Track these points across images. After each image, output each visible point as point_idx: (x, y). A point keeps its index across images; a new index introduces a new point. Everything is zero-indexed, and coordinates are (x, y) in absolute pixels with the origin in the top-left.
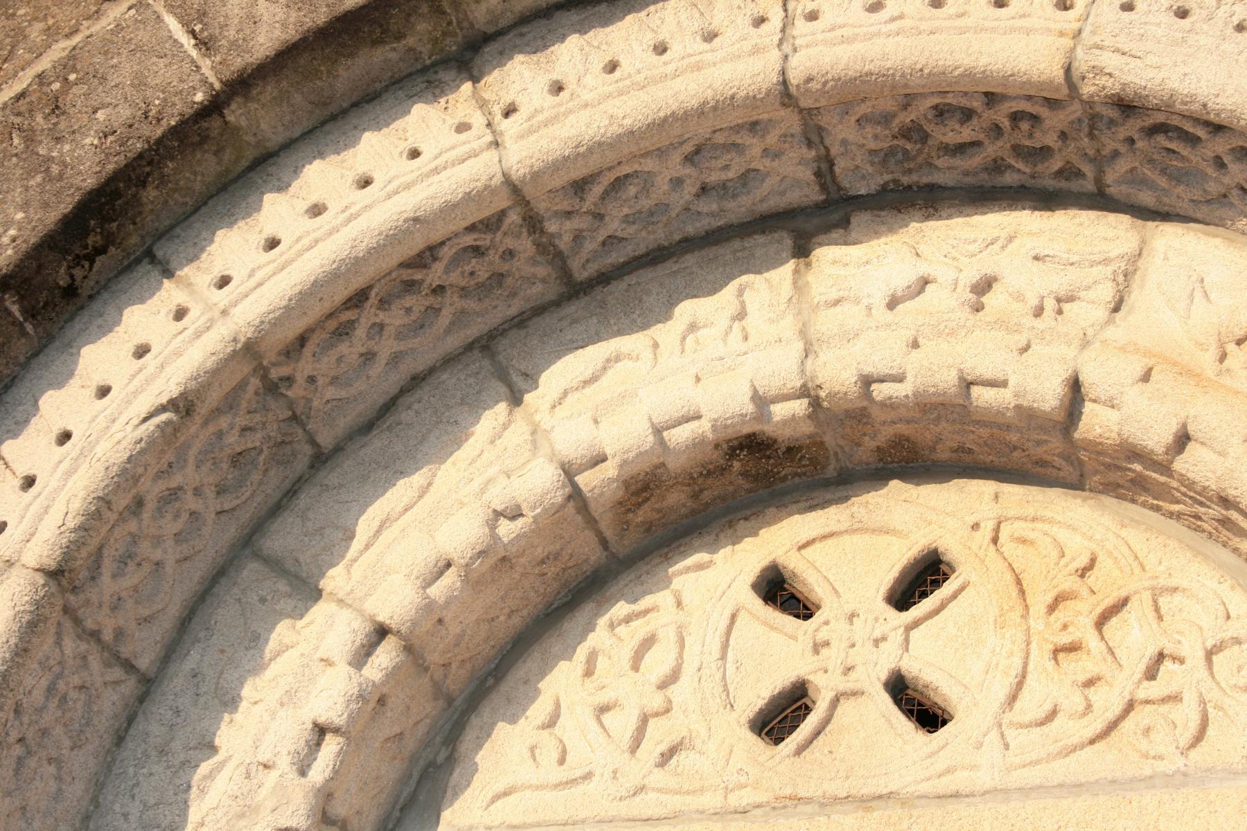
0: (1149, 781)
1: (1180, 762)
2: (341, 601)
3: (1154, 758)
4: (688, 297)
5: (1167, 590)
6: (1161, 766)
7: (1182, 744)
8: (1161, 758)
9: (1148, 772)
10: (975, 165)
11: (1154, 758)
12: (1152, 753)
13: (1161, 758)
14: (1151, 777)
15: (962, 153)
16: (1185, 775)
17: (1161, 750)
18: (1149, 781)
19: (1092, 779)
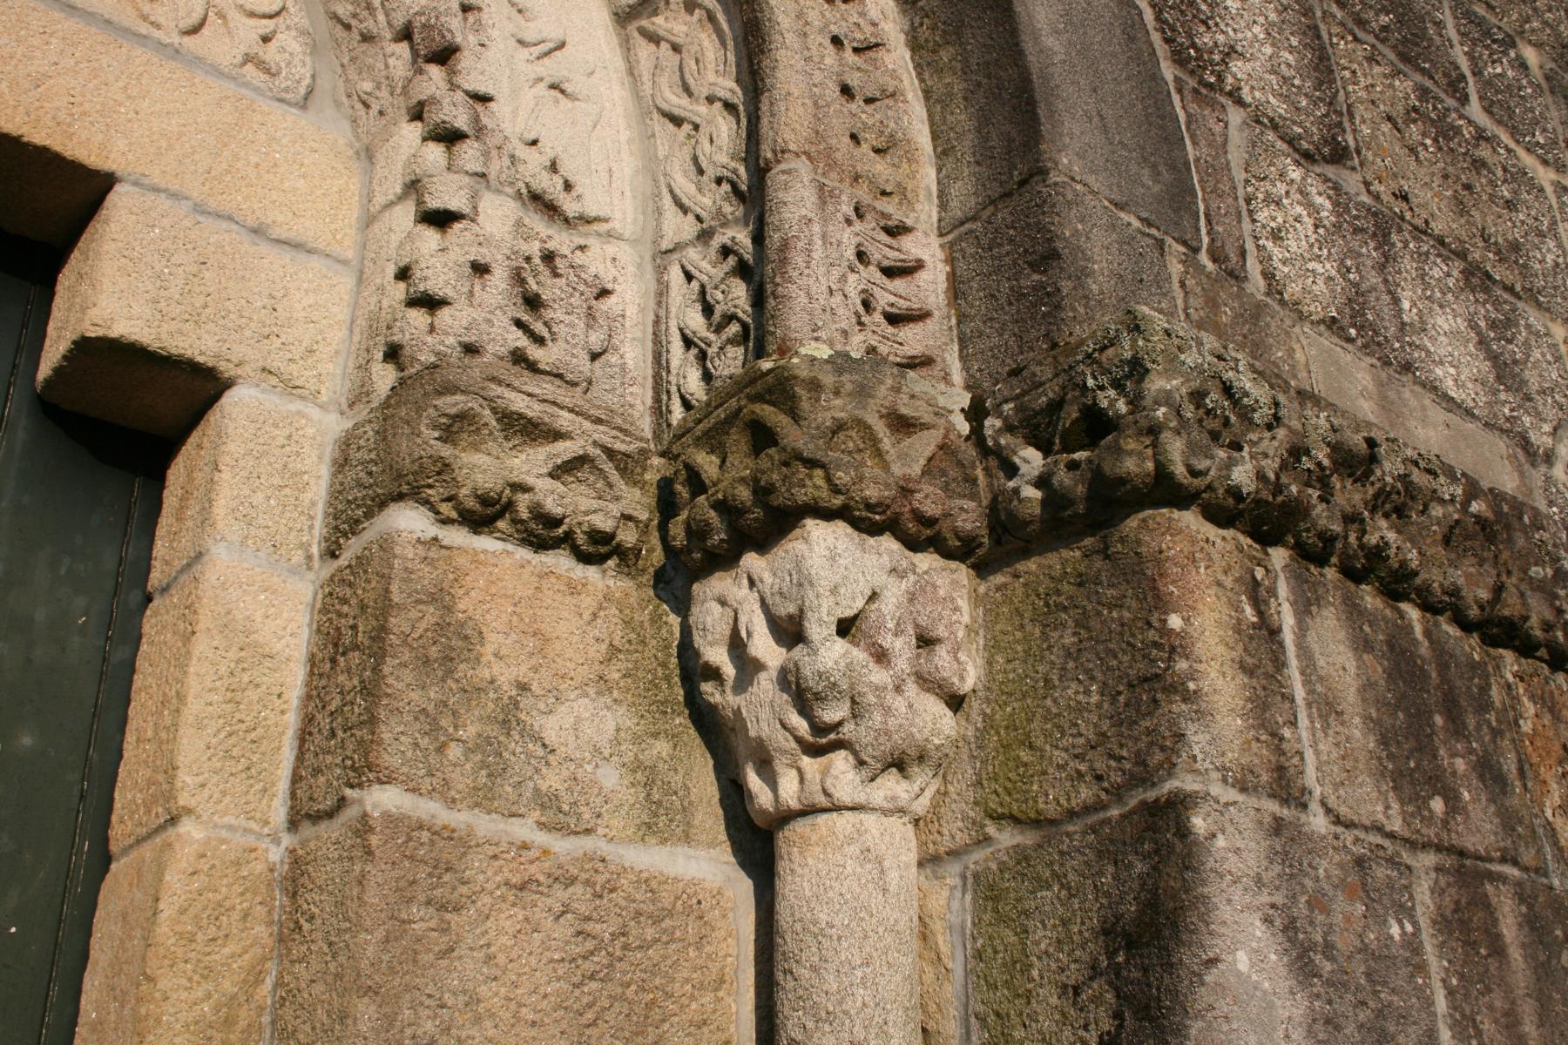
0: (143, 39)
1: (176, 39)
2: (136, 184)
3: (152, 23)
4: (755, 885)
5: (566, 220)
6: (157, 34)
7: (181, 26)
8: (158, 26)
9: (143, 31)
10: (438, 805)
11: (152, 23)
12: (152, 18)
13: (158, 26)
14: (145, 37)
15: (814, 806)
16: (177, 51)
17: (162, 20)
18: (143, 39)
19: (90, 10)
